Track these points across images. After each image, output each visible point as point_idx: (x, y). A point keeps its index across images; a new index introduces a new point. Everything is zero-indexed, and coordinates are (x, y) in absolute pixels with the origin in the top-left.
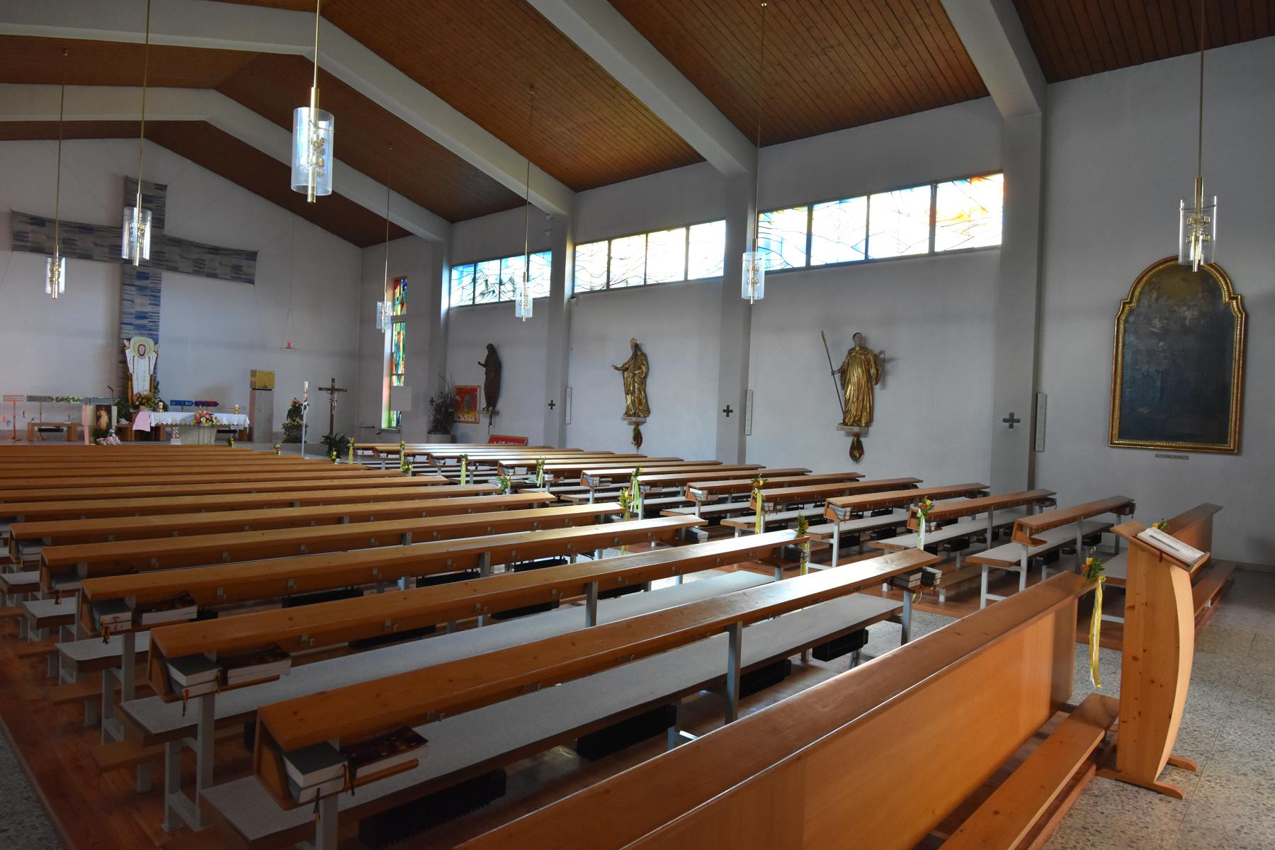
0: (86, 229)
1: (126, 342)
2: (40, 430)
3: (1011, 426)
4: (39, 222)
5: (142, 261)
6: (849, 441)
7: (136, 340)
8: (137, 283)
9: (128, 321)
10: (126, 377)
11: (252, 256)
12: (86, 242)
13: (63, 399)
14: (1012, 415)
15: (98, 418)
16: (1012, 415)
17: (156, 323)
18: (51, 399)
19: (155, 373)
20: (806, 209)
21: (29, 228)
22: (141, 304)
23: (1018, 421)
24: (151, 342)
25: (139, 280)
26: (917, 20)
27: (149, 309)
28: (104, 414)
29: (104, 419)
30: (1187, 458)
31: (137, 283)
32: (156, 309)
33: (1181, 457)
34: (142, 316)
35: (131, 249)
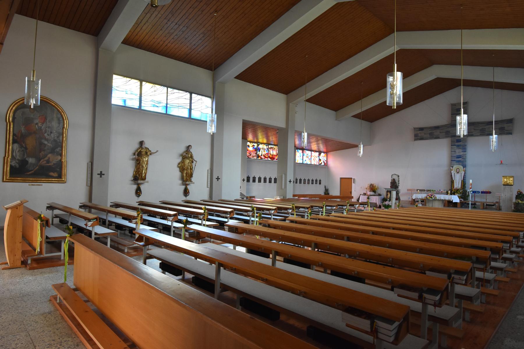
0: (437, 128)
1: (451, 168)
2: (487, 205)
3: (101, 177)
4: (421, 129)
5: (464, 136)
6: (135, 187)
7: (455, 167)
8: (457, 144)
9: (454, 159)
10: (452, 182)
11: (510, 121)
12: (437, 133)
13: (429, 191)
14: (101, 172)
15: (387, 195)
16: (101, 172)
17: (465, 159)
18: (424, 190)
19: (464, 179)
20: (143, 108)
21: (419, 132)
22: (459, 152)
23: (104, 175)
24: (462, 167)
25: (458, 143)
26: (159, 15)
27: (462, 154)
28: (389, 193)
29: (389, 195)
30: (42, 185)
31: (457, 144)
32: (465, 153)
33: (39, 185)
34: (459, 157)
35: (460, 132)
